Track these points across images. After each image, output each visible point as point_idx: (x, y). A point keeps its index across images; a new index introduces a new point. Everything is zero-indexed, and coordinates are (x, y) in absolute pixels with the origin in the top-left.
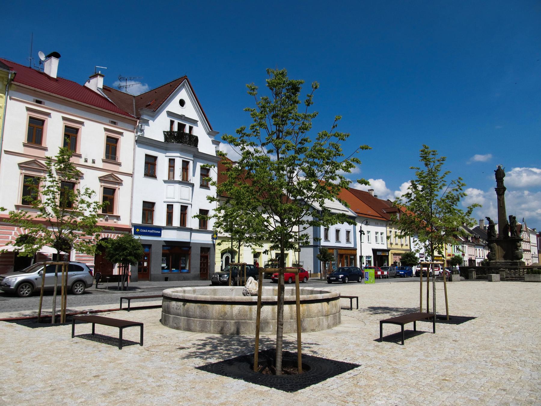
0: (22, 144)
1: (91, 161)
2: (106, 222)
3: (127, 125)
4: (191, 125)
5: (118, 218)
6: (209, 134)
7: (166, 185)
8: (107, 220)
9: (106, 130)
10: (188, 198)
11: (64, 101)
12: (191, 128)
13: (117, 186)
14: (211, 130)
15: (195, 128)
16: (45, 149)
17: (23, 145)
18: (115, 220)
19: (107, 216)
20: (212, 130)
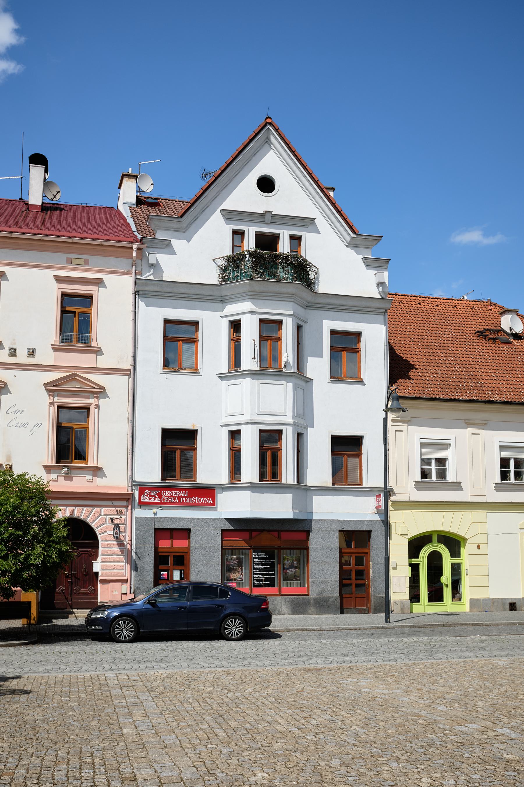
0: (51, 347)
1: (18, 353)
2: (68, 483)
3: (113, 261)
4: (296, 232)
5: (97, 471)
6: (351, 245)
7: (225, 383)
8: (68, 477)
9: (59, 279)
10: (282, 411)
11: (72, 245)
12: (296, 240)
13: (92, 401)
14: (355, 236)
15: (308, 238)
16: (98, 351)
17: (52, 348)
18: (89, 477)
19: (66, 469)
20: (357, 235)
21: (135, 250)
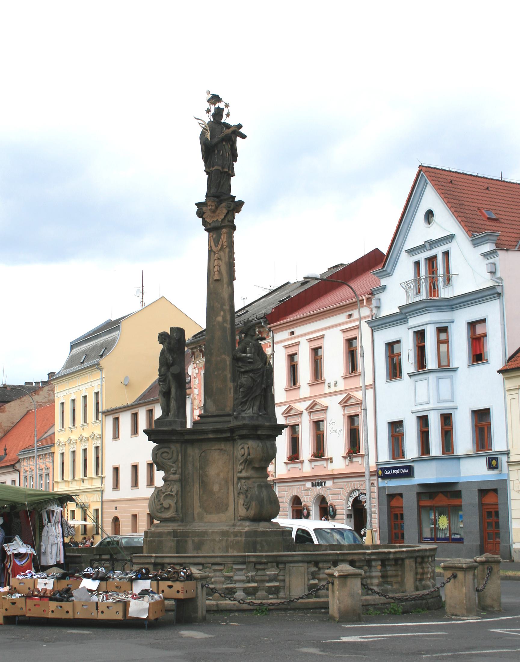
21: (365, 301)
